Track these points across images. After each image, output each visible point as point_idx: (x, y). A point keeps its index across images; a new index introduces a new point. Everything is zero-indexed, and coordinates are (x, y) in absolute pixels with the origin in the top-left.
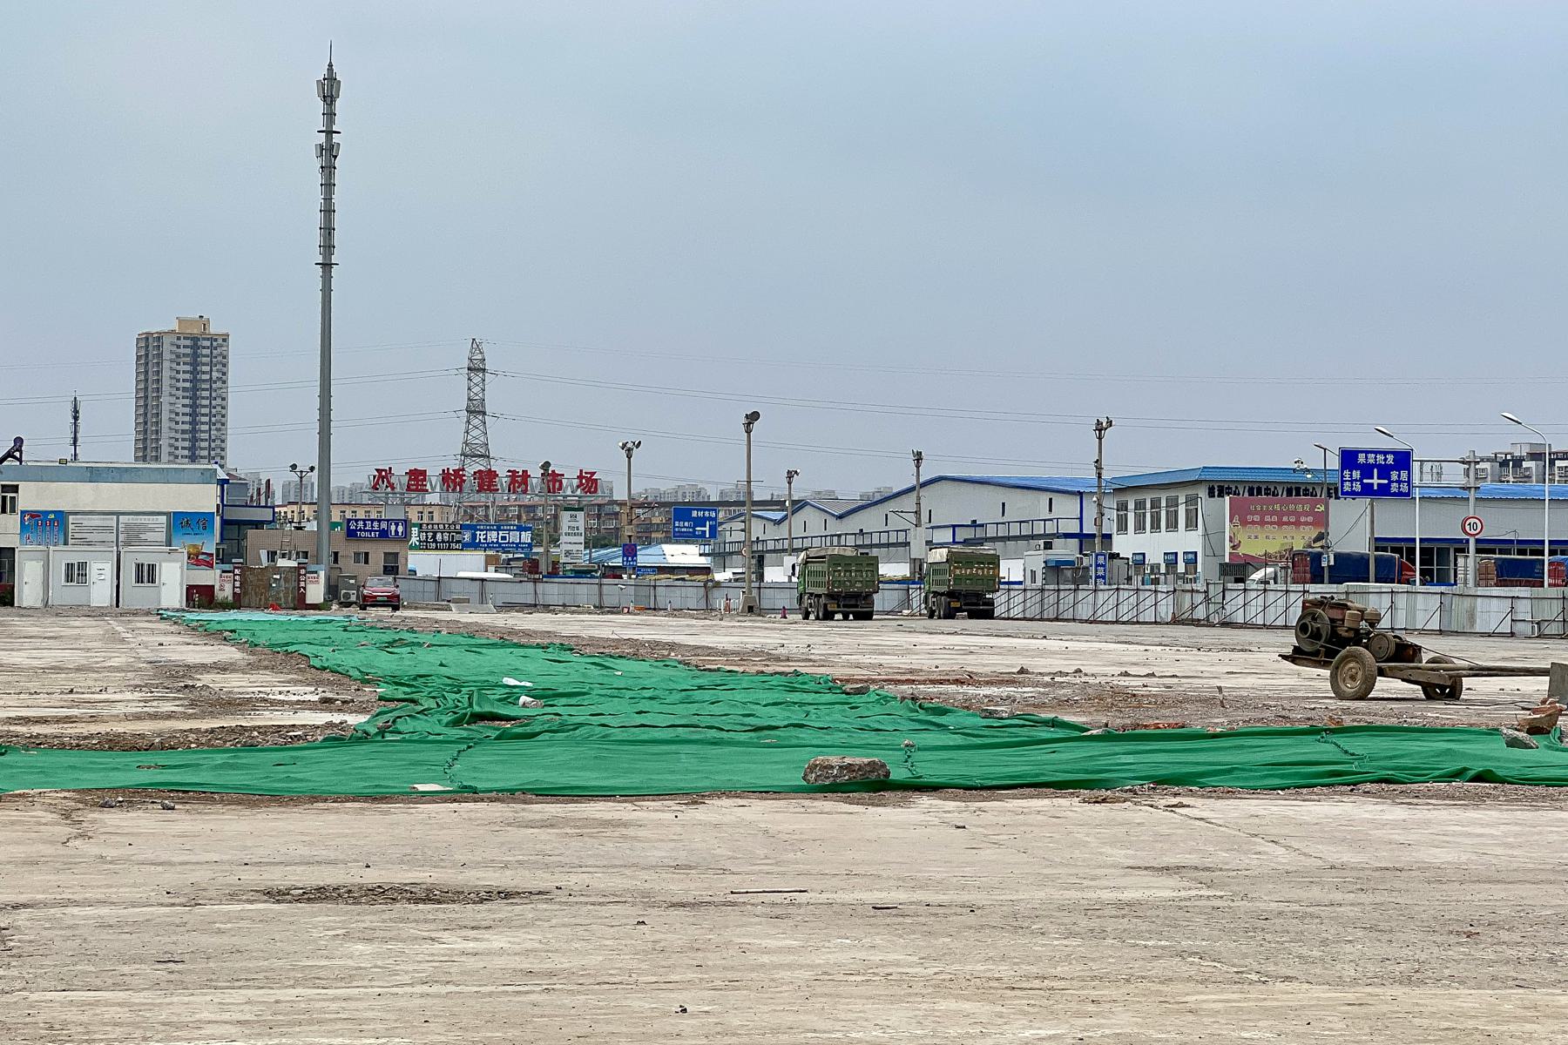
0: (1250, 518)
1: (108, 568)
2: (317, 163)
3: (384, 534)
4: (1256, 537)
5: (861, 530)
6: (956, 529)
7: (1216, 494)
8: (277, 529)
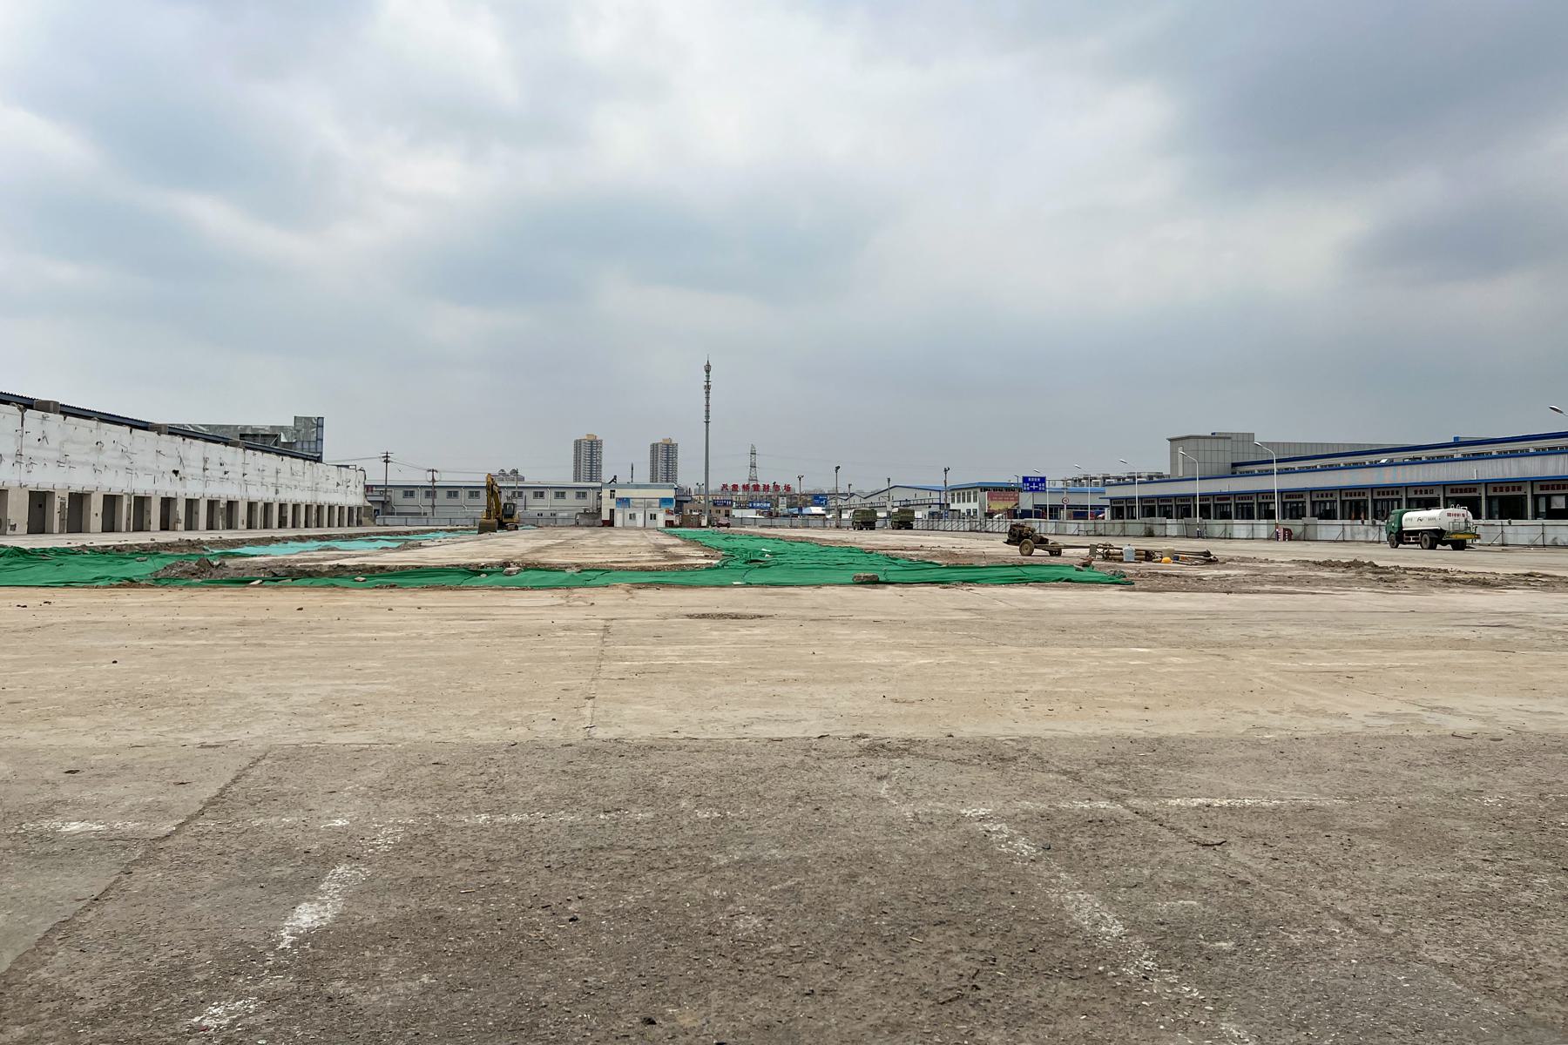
1: (642, 515)
2: (704, 391)
3: (725, 504)
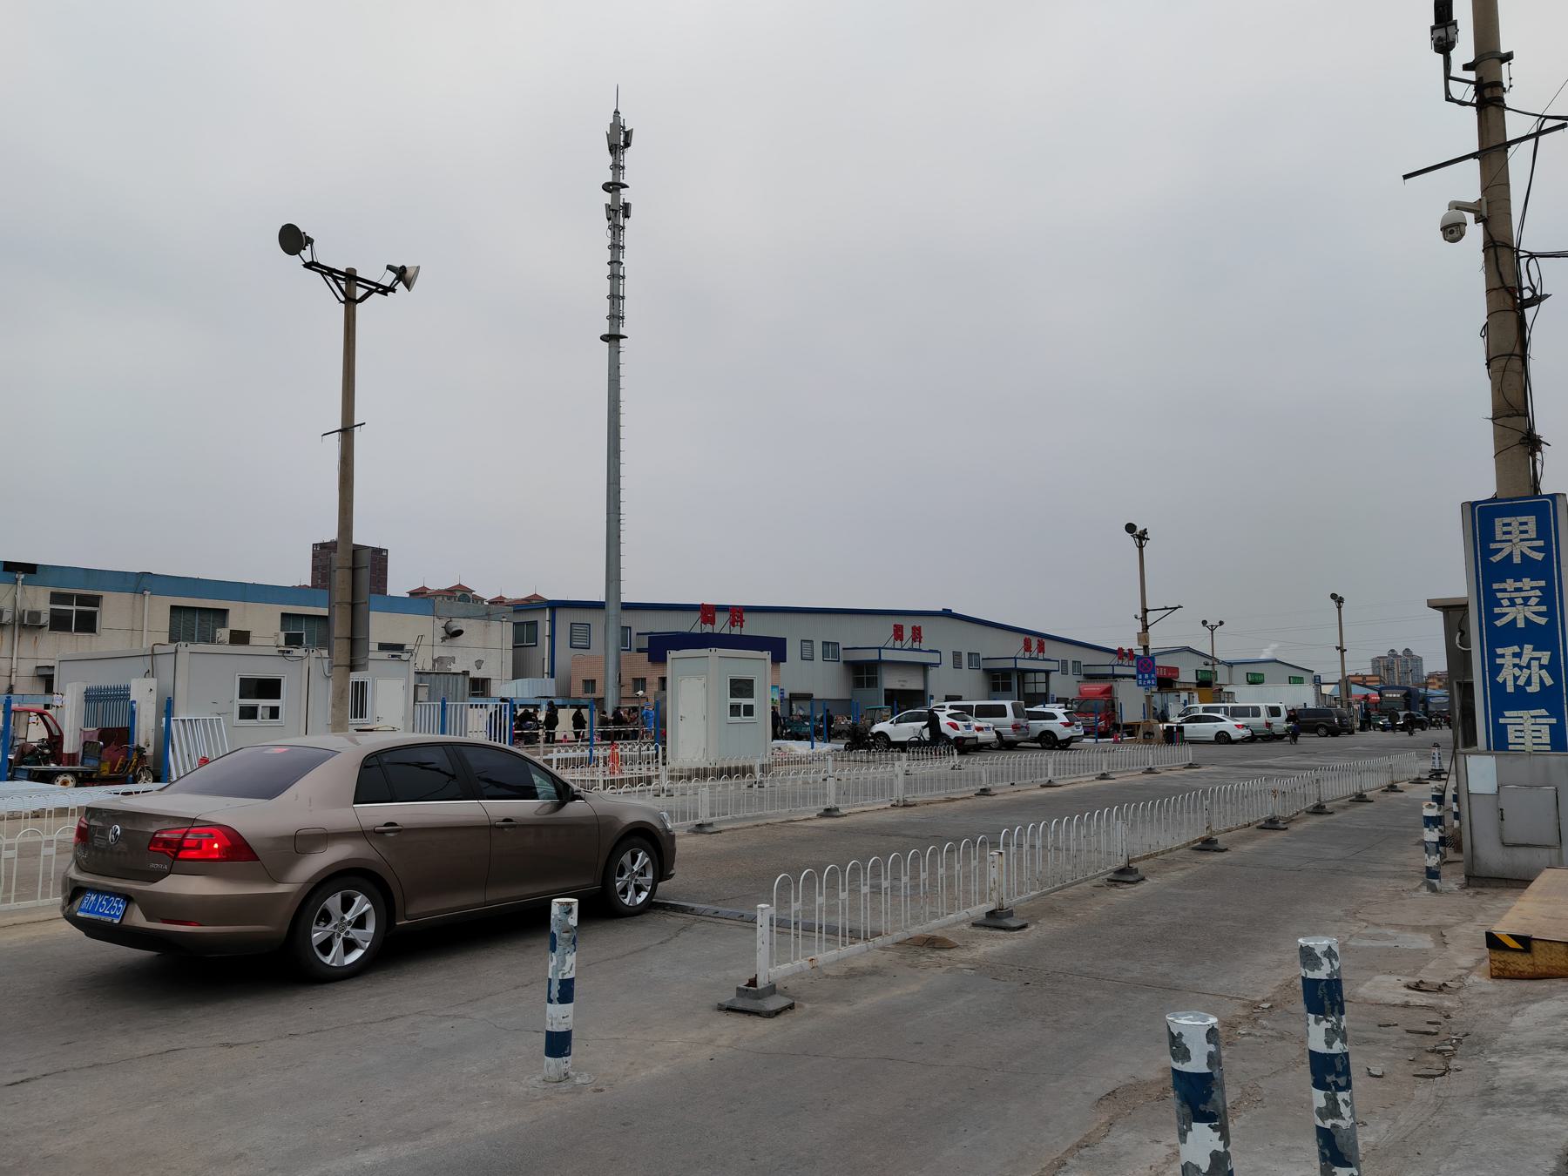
5: (1337, 648)
6: (882, 650)
8: (1048, 741)
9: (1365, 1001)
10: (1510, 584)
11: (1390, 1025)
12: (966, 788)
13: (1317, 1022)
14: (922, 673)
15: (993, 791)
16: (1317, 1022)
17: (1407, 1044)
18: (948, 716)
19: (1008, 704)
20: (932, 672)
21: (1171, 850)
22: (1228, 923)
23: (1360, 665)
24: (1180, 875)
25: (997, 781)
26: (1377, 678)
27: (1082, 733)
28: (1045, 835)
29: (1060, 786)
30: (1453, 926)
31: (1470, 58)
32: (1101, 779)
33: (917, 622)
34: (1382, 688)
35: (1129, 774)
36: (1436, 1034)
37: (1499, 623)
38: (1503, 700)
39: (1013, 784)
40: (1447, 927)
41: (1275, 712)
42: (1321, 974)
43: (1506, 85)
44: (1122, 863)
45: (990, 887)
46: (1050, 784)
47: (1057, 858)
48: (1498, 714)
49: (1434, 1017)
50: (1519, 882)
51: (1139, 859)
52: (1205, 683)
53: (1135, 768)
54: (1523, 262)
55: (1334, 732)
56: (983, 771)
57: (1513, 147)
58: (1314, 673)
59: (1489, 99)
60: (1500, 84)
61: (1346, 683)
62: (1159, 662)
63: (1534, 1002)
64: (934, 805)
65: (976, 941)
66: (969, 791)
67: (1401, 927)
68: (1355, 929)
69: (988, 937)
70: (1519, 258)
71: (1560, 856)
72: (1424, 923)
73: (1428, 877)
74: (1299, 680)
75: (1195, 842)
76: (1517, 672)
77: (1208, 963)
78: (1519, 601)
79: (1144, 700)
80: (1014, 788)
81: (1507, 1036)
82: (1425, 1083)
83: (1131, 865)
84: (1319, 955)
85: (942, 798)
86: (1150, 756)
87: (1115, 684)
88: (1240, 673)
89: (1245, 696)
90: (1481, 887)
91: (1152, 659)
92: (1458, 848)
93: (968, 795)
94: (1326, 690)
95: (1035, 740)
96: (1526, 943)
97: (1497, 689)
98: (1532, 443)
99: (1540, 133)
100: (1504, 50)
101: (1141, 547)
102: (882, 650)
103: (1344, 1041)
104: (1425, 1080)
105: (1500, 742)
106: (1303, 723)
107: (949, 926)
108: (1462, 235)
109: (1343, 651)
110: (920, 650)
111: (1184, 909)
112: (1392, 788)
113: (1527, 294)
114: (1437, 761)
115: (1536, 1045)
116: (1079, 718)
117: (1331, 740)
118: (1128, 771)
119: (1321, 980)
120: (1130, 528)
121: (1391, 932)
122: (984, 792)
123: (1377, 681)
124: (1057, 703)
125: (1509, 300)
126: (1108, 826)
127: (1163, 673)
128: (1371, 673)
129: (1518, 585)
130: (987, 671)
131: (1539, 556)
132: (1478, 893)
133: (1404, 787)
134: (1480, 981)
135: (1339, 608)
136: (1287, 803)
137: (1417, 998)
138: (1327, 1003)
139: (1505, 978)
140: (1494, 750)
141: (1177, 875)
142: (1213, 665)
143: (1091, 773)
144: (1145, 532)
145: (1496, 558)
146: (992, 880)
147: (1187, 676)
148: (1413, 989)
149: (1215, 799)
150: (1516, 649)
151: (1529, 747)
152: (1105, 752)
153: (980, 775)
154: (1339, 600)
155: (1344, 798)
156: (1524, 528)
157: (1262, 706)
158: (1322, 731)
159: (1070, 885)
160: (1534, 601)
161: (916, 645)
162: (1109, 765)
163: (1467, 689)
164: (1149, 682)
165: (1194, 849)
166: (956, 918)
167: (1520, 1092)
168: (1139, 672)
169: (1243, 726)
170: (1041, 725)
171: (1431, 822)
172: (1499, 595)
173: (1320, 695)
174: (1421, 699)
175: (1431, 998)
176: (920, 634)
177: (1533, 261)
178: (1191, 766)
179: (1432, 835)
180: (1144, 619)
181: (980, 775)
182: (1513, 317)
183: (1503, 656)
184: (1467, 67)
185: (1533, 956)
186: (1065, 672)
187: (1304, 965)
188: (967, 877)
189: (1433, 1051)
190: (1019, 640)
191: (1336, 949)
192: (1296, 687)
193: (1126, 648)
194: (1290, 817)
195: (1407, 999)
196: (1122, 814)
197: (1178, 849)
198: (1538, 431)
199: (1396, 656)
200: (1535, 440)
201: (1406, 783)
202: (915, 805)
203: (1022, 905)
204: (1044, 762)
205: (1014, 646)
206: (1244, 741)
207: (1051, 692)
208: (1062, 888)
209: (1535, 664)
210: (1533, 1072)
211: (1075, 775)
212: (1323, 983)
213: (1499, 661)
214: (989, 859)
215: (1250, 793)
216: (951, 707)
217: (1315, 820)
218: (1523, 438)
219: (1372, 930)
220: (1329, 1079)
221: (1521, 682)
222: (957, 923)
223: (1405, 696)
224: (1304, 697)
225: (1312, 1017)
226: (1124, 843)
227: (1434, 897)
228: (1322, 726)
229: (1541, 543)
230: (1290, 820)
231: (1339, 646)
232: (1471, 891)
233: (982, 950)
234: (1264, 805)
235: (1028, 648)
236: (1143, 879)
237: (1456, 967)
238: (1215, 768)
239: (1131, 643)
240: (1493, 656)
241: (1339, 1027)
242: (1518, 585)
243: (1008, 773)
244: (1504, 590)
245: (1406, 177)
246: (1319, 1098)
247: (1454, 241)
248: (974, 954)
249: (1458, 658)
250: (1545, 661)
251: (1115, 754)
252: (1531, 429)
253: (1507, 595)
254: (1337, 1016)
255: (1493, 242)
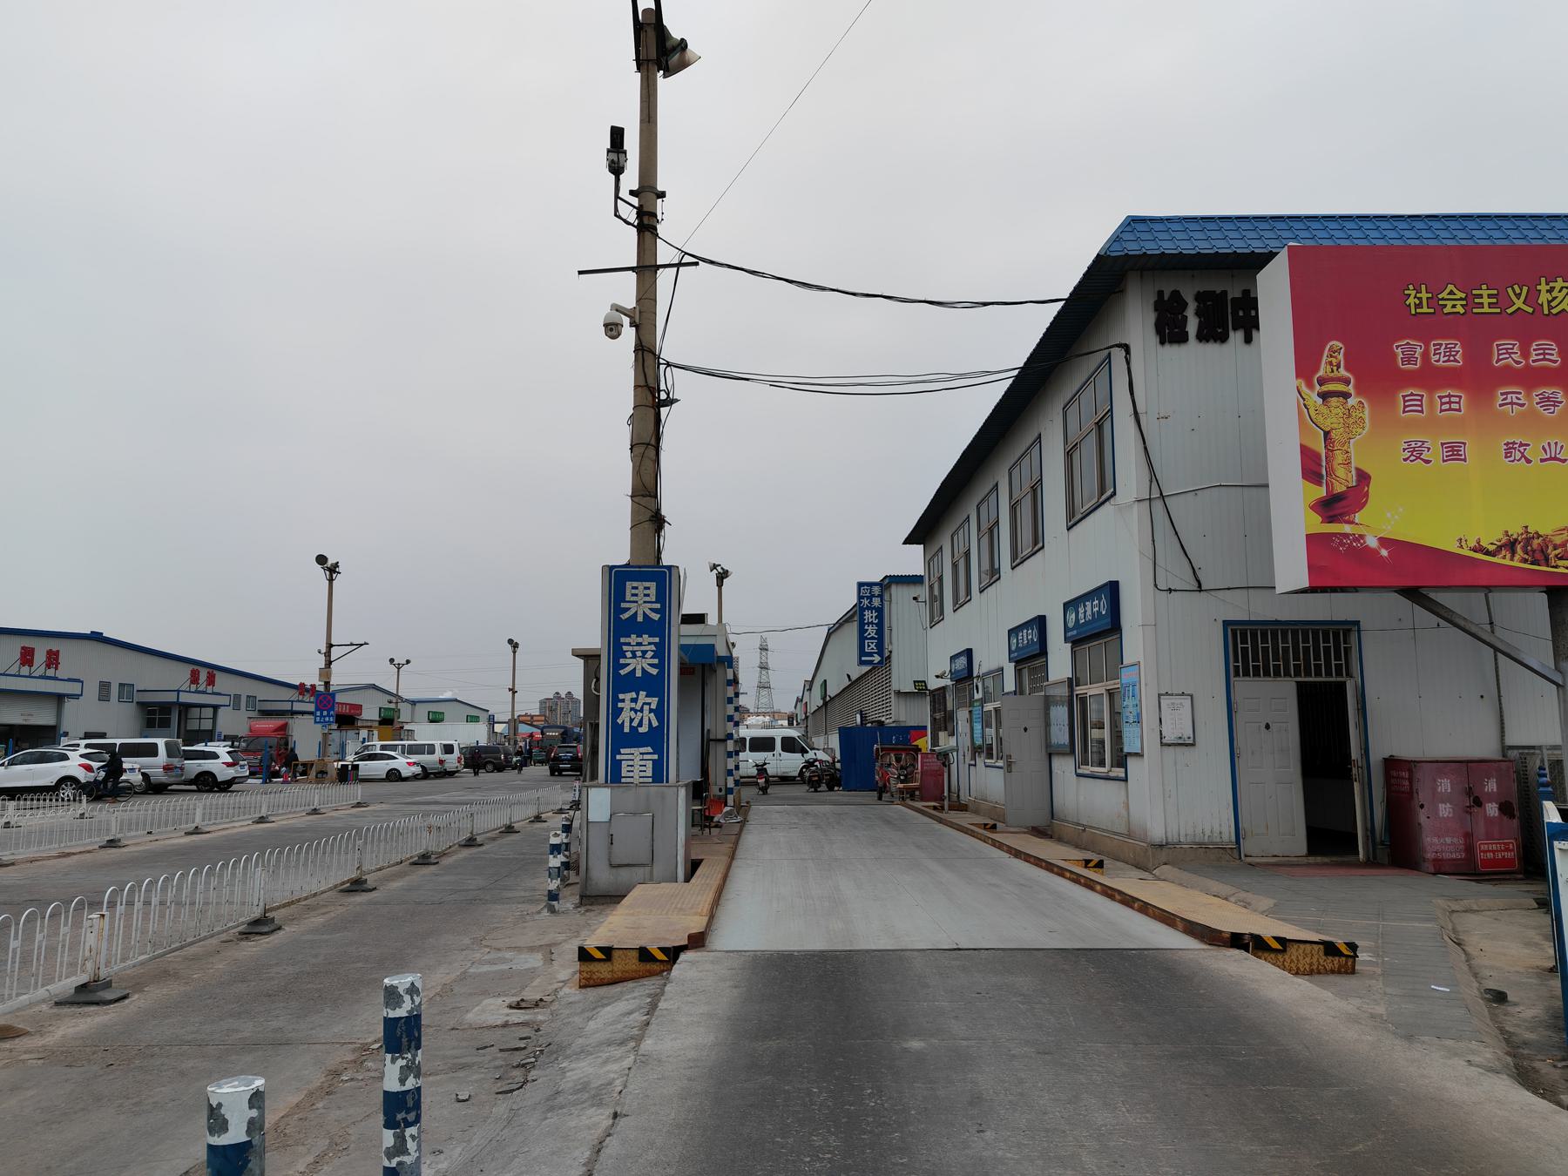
0: (1406, 352)
4: (1454, 452)
5: (510, 690)
6: (181, 693)
7: (1192, 326)
8: (207, 783)
9: (471, 1027)
10: (633, 639)
11: (486, 1047)
12: (88, 841)
13: (393, 1061)
14: (56, 705)
15: (124, 842)
16: (393, 1061)
17: (497, 1063)
18: (81, 756)
19: (161, 743)
20: (69, 705)
21: (315, 895)
22: (360, 965)
23: (529, 705)
24: (321, 920)
25: (130, 830)
26: (543, 718)
27: (248, 773)
28: (164, 889)
29: (209, 832)
30: (560, 943)
31: (635, 187)
32: (258, 823)
33: (54, 645)
34: (544, 727)
35: (291, 816)
36: (525, 1048)
37: (623, 672)
38: (622, 739)
39: (150, 833)
40: (555, 944)
41: (448, 749)
42: (401, 1012)
43: (659, 218)
44: (257, 913)
45: (83, 956)
46: (197, 831)
47: (177, 915)
48: (616, 751)
49: (526, 1032)
50: (613, 898)
51: (278, 908)
52: (388, 721)
53: (298, 809)
54: (662, 367)
55: (499, 768)
56: (113, 819)
57: (661, 270)
58: (489, 713)
59: (646, 225)
60: (655, 216)
61: (514, 723)
62: (339, 698)
63: (607, 1005)
64: (40, 863)
65: (54, 1023)
66: (91, 843)
67: (518, 949)
68: (478, 955)
69: (73, 1016)
70: (659, 364)
71: (651, 873)
72: (538, 943)
73: (549, 900)
74: (473, 719)
75: (343, 883)
76: (633, 714)
77: (327, 1010)
78: (639, 654)
79: (320, 738)
80: (151, 837)
81: (580, 1041)
82: (504, 1099)
83: (267, 915)
84: (402, 993)
85: (54, 853)
86: (317, 797)
87: (290, 721)
88: (422, 711)
89: (425, 733)
90: (591, 905)
91: (333, 695)
92: (577, 869)
93: (90, 848)
94: (499, 728)
95: (190, 782)
96: (608, 952)
97: (616, 728)
98: (658, 521)
99: (679, 265)
100: (660, 188)
101: (331, 580)
102: (181, 693)
103: (417, 1076)
104: (504, 1095)
105: (615, 777)
106: (477, 759)
107: (18, 1009)
108: (619, 335)
109: (514, 692)
110: (55, 678)
111: (316, 956)
112: (538, 819)
113: (663, 396)
114: (577, 793)
115: (600, 1044)
116: (245, 758)
117: (496, 775)
118: (290, 813)
119: (401, 1018)
120: (321, 560)
121: (508, 955)
122: (112, 843)
123: (542, 721)
124: (224, 740)
125: (650, 398)
126: (245, 874)
127: (345, 710)
128: (538, 714)
129: (640, 640)
130: (142, 705)
131: (656, 617)
132: (587, 911)
133: (549, 817)
134: (571, 992)
135: (514, 652)
136: (441, 839)
137: (518, 1016)
138: (404, 1040)
139: (590, 987)
140: (611, 782)
141: (317, 920)
142: (397, 703)
143: (246, 817)
144: (337, 565)
145: (625, 616)
146: (87, 948)
147: (370, 713)
148: (514, 1008)
149: (369, 839)
150: (634, 695)
151: (636, 780)
152: (266, 794)
153: (108, 824)
154: (514, 645)
155: (496, 829)
156: (647, 592)
157: (437, 744)
158: (490, 767)
159: (192, 943)
160: (650, 654)
161: (51, 672)
162: (269, 807)
163: (595, 727)
164: (327, 719)
165: (342, 891)
166: (30, 998)
167: (579, 1091)
168: (317, 710)
169: (414, 763)
170: (200, 765)
171: (555, 849)
172: (625, 648)
173: (492, 732)
174: (574, 737)
175: (527, 1014)
176: (57, 659)
177: (669, 369)
178: (359, 805)
179: (555, 861)
180: (328, 654)
181: (108, 824)
182: (651, 412)
183: (623, 701)
184: (632, 193)
185: (612, 964)
186: (237, 707)
187: (387, 1005)
188: (52, 950)
189: (518, 1066)
190: (186, 670)
191: (418, 985)
192: (472, 725)
193: (308, 683)
194: (443, 851)
195: (508, 1018)
196: (263, 861)
197: (323, 892)
198: (663, 512)
199: (560, 698)
200: (661, 519)
201: (550, 814)
202: (13, 864)
203: (128, 972)
204: (191, 807)
205: (181, 676)
206: (415, 777)
207: (218, 729)
208: (182, 948)
209: (646, 708)
210: (591, 1070)
211: (228, 820)
212: (403, 1021)
213: (620, 705)
214: (86, 924)
215: (405, 829)
216: (87, 746)
217: (466, 852)
218: (652, 516)
219: (493, 955)
220: (399, 1117)
221: (635, 724)
222: (31, 1005)
223: (562, 734)
224: (477, 735)
225: (389, 1056)
226: (262, 892)
227: (554, 918)
228: (490, 762)
229: (658, 606)
230: (443, 854)
231: (511, 687)
232: (582, 909)
233: (60, 1033)
234: (418, 841)
235: (195, 678)
236: (280, 928)
237: (555, 981)
238: (383, 805)
239: (312, 679)
240: (616, 700)
241: (413, 1063)
242: (640, 640)
243: (146, 820)
244: (629, 644)
245: (580, 273)
246: (388, 1137)
247: (613, 338)
248: (47, 1040)
249: (592, 701)
250: (653, 706)
251: (282, 795)
252: (659, 510)
253: (631, 648)
254: (413, 1052)
255: (642, 346)
